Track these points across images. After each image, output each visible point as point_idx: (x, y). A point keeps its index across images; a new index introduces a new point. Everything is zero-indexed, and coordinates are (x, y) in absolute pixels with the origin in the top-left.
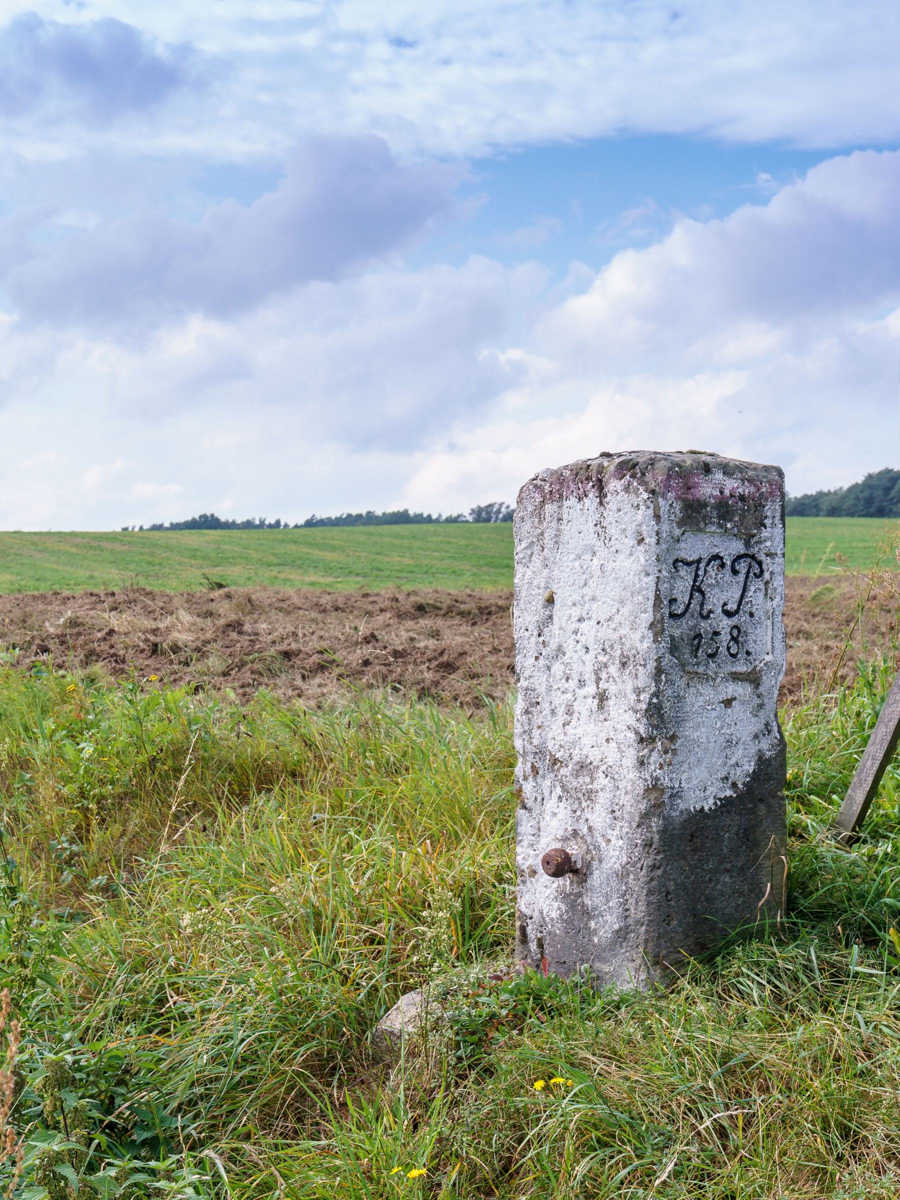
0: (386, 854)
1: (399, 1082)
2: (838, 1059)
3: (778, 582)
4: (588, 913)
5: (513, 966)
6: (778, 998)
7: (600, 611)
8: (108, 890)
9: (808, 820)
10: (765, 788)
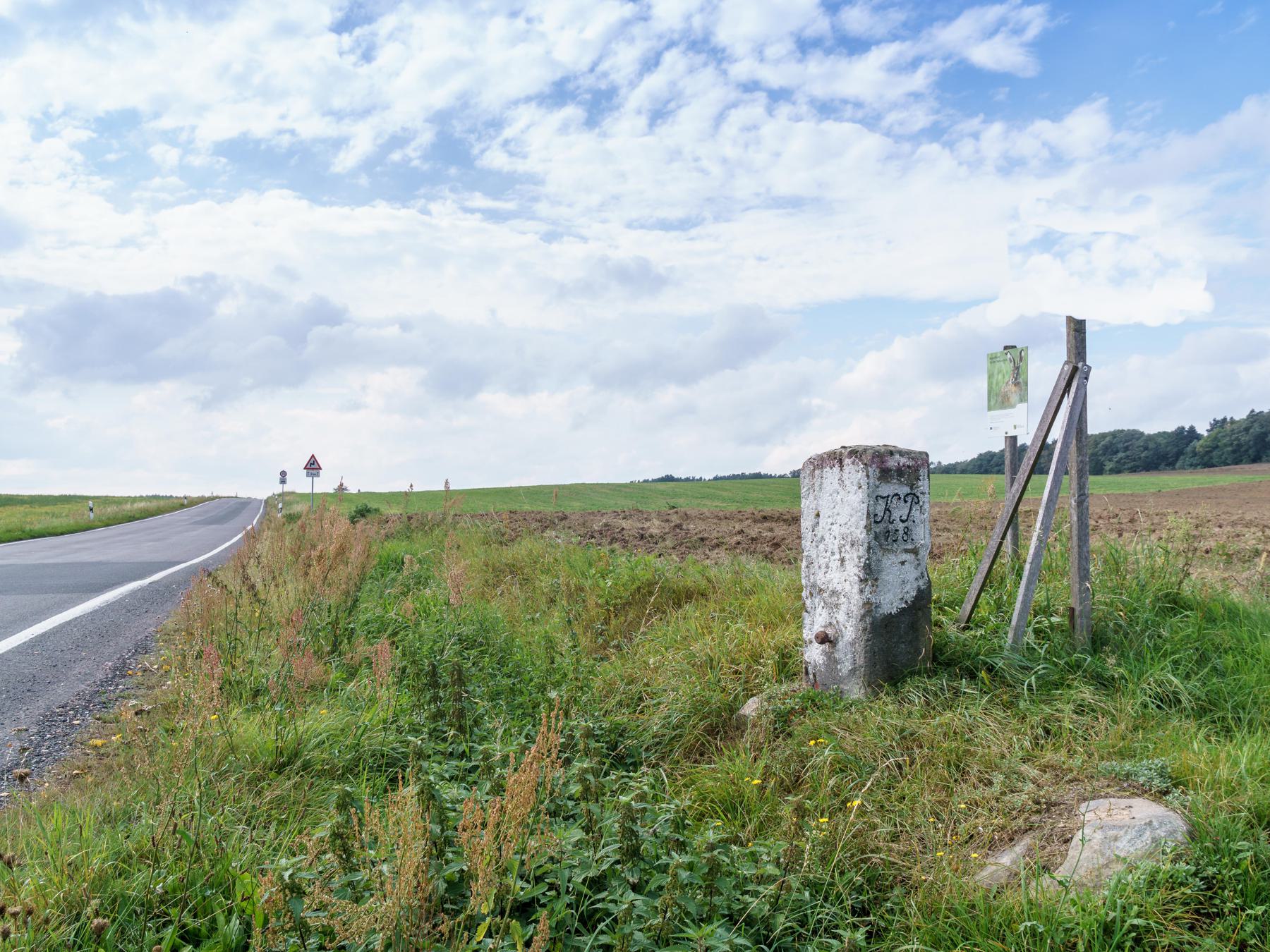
0: (744, 632)
1: (747, 740)
2: (955, 733)
3: (927, 506)
4: (836, 662)
5: (801, 686)
6: (928, 704)
7: (841, 520)
8: (618, 647)
9: (943, 619)
10: (921, 602)
